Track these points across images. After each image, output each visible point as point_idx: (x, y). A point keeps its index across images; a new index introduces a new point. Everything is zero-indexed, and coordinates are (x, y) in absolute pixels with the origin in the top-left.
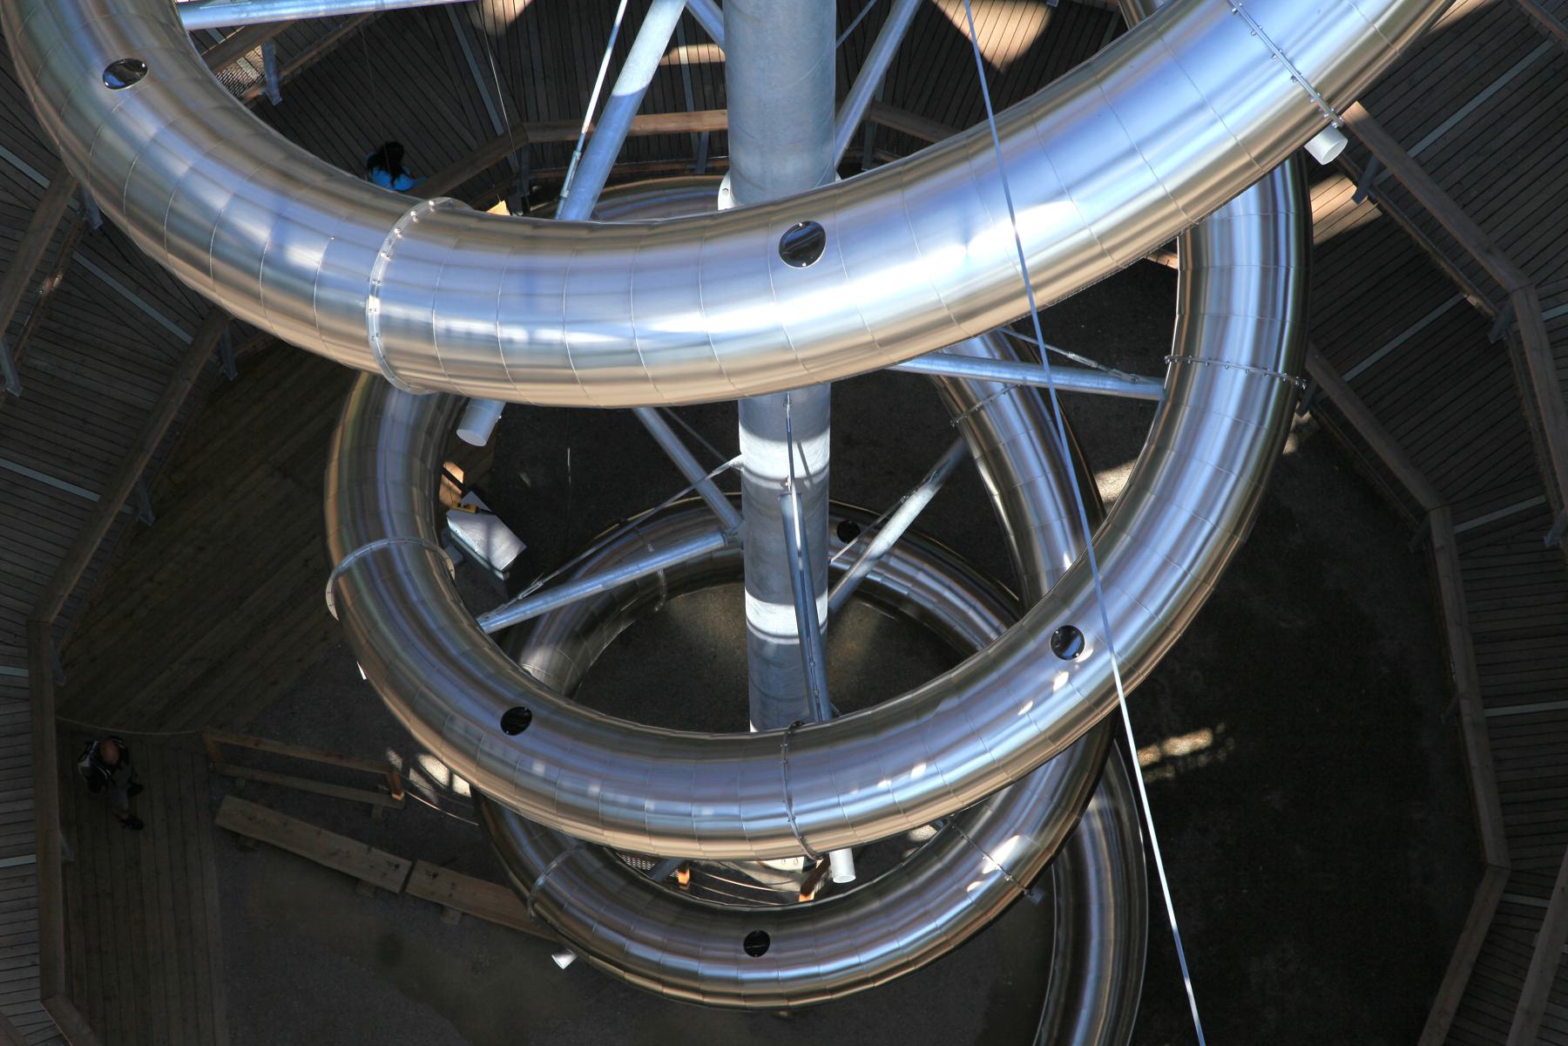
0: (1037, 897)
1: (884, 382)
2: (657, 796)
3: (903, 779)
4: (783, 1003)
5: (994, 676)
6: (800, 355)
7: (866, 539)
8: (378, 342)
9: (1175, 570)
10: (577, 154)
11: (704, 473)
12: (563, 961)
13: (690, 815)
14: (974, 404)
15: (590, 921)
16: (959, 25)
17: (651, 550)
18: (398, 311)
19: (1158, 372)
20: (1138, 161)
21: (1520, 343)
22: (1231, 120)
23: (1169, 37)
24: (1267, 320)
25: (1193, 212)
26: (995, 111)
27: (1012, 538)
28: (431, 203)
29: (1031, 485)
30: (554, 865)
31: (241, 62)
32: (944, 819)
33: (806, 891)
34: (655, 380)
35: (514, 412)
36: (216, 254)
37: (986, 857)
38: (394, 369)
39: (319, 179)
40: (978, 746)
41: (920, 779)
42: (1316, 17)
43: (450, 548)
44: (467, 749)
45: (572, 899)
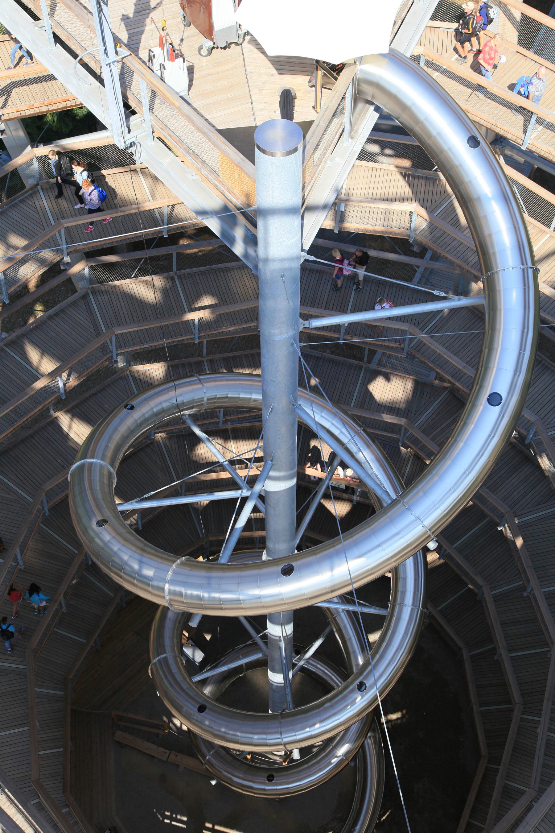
0: (353, 764)
2: (242, 732)
3: (312, 728)
4: (278, 797)
5: (340, 696)
6: (287, 602)
7: (303, 655)
8: (167, 597)
9: (392, 665)
10: (224, 544)
11: (256, 634)
12: (213, 783)
13: (252, 738)
14: (333, 615)
15: (221, 770)
17: (241, 657)
18: (172, 588)
19: (386, 607)
20: (381, 548)
21: (485, 600)
24: (416, 592)
25: (396, 563)
26: (342, 533)
27: (345, 655)
28: (184, 558)
29: (350, 639)
30: (211, 753)
31: (132, 519)
32: (326, 740)
33: (285, 762)
34: (245, 608)
35: (205, 617)
36: (124, 573)
37: (338, 751)
38: (172, 605)
39: (153, 552)
40: (336, 718)
41: (318, 728)
42: (428, 510)
43: (184, 656)
44: (188, 717)
45: (217, 764)
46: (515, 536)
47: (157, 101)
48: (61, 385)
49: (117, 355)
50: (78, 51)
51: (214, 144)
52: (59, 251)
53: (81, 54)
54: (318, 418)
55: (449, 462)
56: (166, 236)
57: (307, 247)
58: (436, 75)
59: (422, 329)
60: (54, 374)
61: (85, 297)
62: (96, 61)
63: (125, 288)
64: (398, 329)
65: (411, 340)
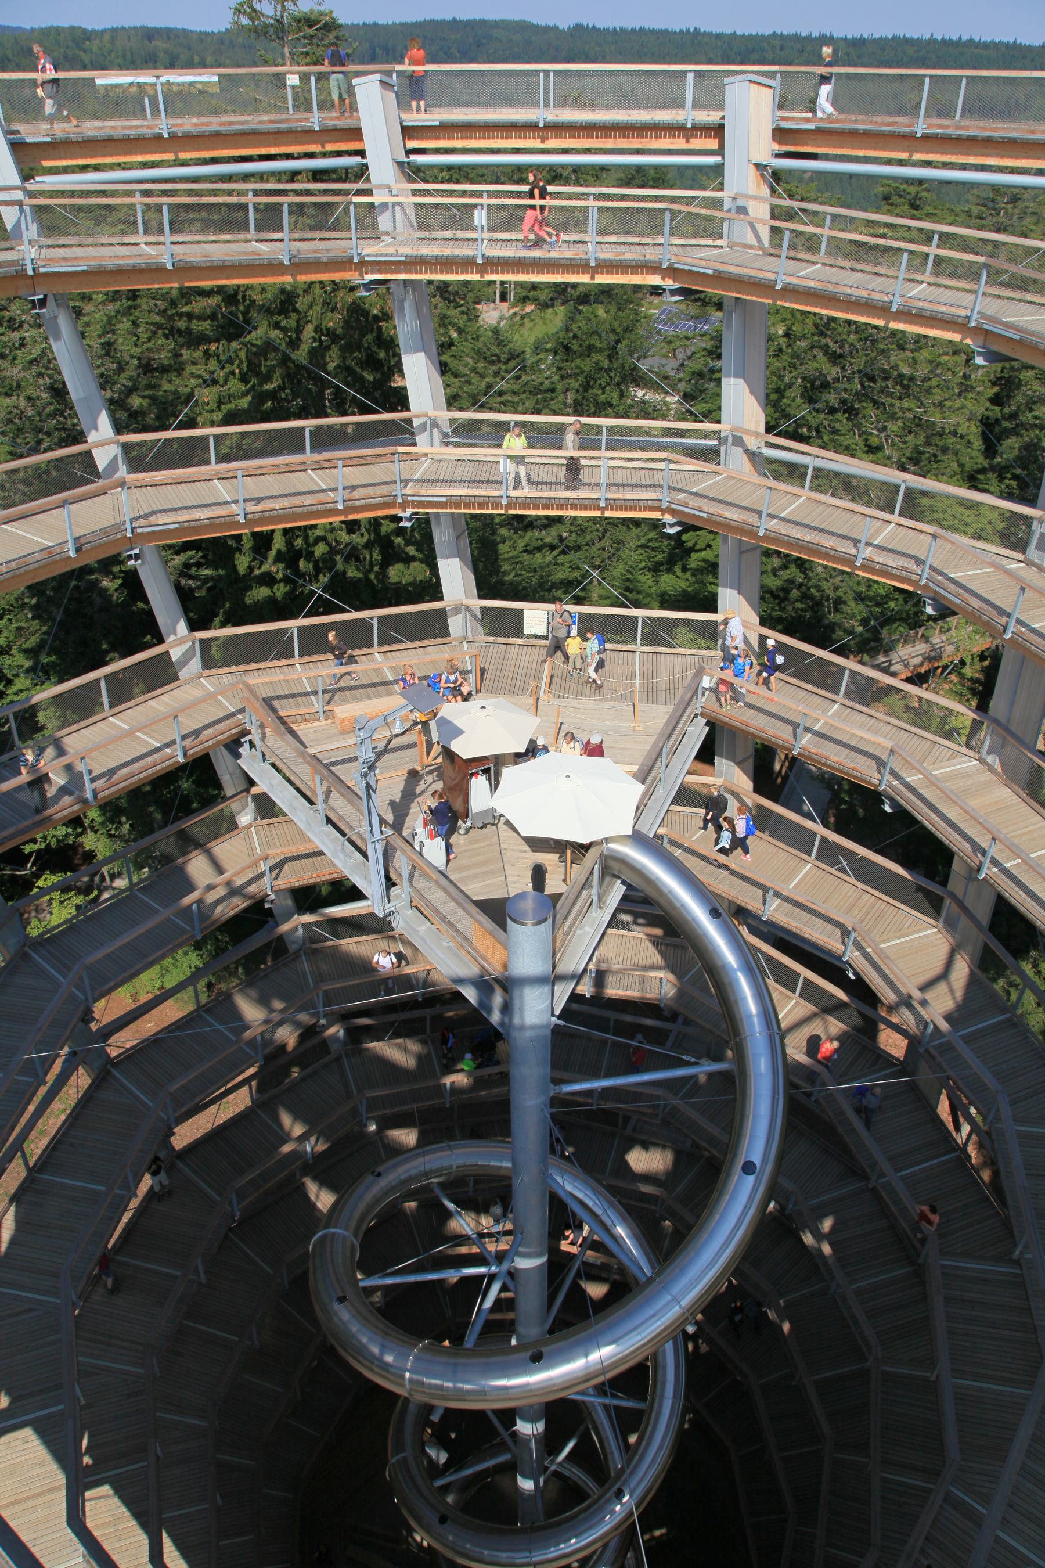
1: (563, 1401)
8: (408, 1386)
16: (653, 739)
18: (415, 1377)
19: (645, 1400)
22: (662, 1320)
23: (644, 1294)
35: (448, 1410)
44: (428, 1530)
46: (782, 1320)
47: (417, 874)
48: (309, 1149)
49: (368, 1119)
50: (347, 831)
51: (468, 913)
52: (316, 1015)
53: (349, 833)
54: (569, 1187)
55: (705, 1236)
56: (420, 999)
57: (557, 1012)
58: (678, 853)
59: (676, 1094)
60: (303, 1138)
61: (338, 1059)
62: (363, 839)
63: (379, 1051)
64: (652, 1095)
65: (665, 1106)
